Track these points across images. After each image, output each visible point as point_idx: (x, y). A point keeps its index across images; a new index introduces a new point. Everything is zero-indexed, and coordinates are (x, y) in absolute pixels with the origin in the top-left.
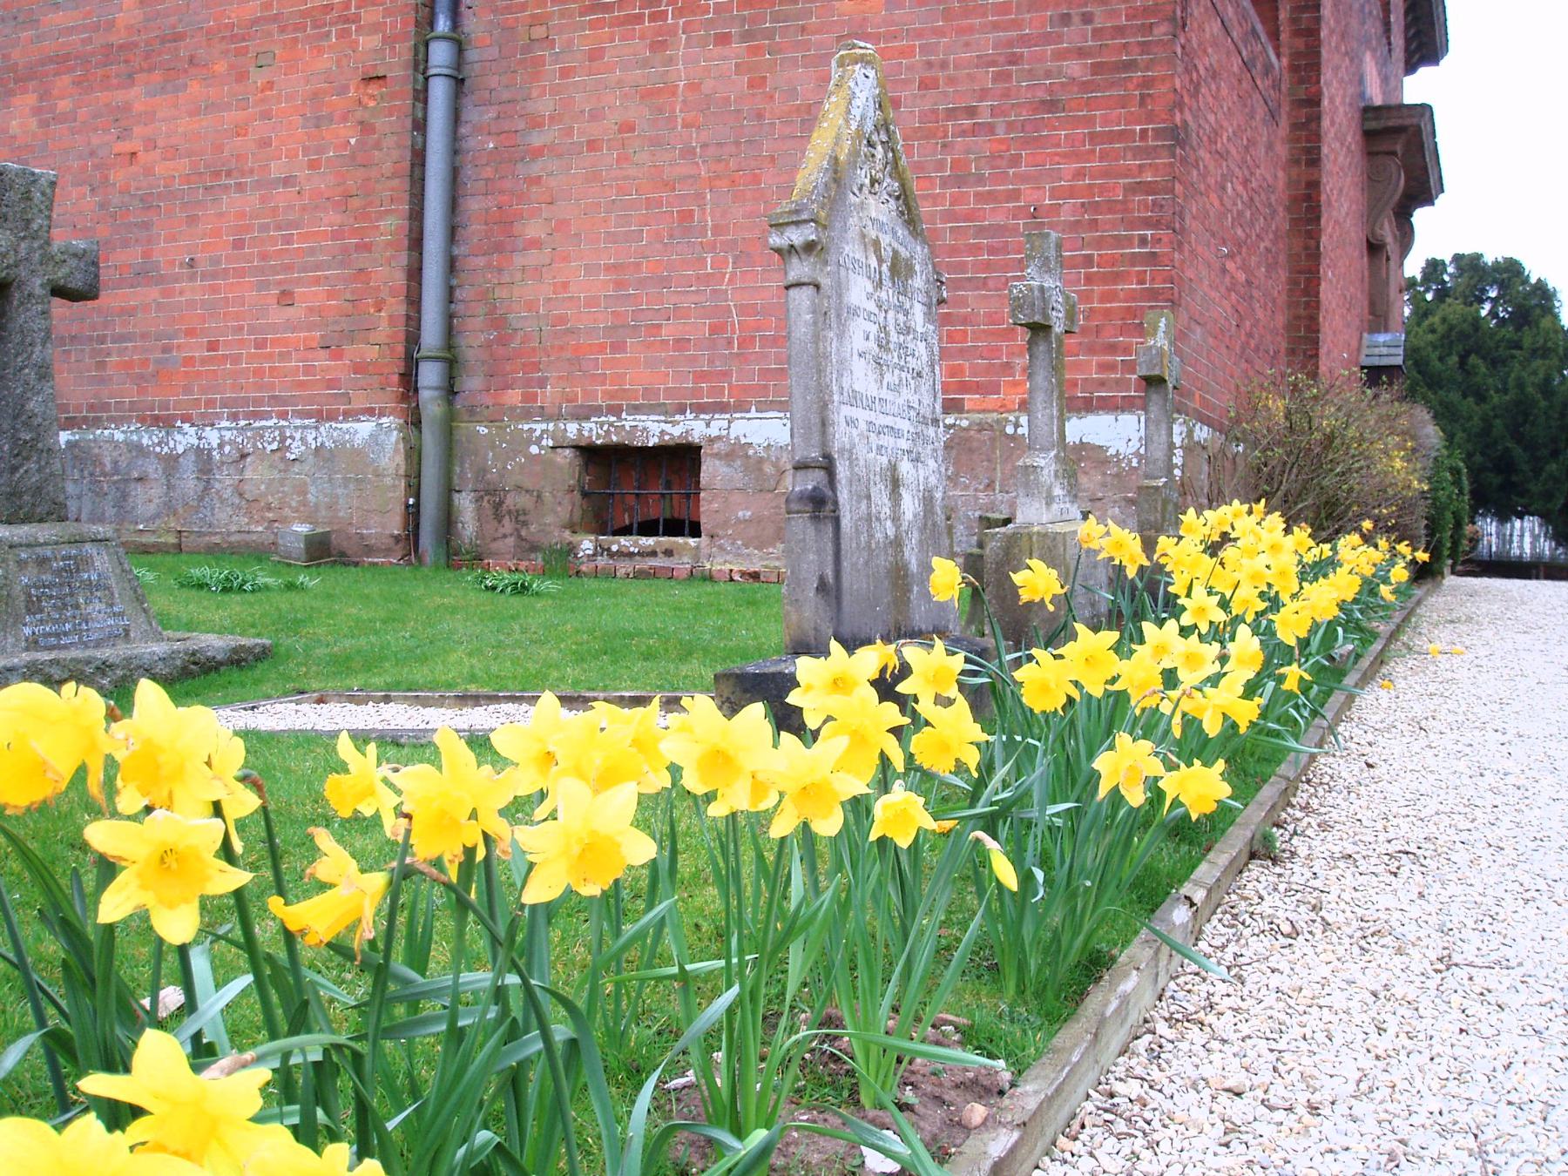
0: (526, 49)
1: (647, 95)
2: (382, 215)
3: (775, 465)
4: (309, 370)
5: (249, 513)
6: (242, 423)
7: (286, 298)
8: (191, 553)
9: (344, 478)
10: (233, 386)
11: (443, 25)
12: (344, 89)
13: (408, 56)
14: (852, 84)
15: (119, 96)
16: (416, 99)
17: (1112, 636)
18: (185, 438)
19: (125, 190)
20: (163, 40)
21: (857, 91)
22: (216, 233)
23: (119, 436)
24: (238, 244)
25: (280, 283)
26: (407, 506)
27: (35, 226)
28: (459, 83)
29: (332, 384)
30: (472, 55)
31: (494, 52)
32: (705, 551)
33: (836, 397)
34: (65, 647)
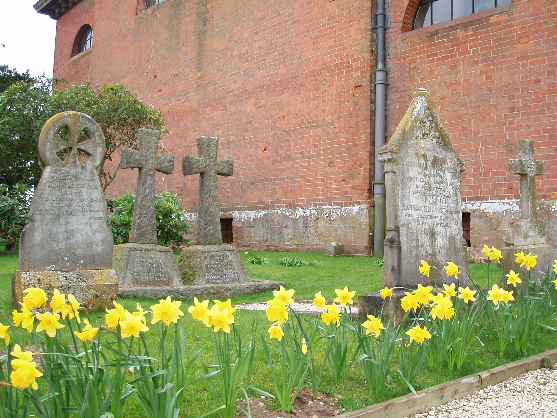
0: (409, 72)
1: (450, 85)
2: (361, 134)
3: (497, 220)
4: (338, 189)
5: (319, 238)
6: (318, 207)
7: (331, 164)
8: (301, 252)
9: (349, 226)
10: (315, 195)
11: (380, 66)
12: (349, 91)
13: (369, 78)
14: (415, 103)
15: (279, 98)
16: (371, 93)
17: (430, 288)
18: (300, 213)
19: (281, 130)
20: (292, 78)
21: (417, 105)
22: (309, 142)
23: (279, 212)
24: (316, 146)
25: (329, 159)
26: (370, 236)
27: (212, 155)
28: (386, 86)
29: (346, 193)
30: (391, 75)
31: (398, 74)
32: (472, 252)
33: (400, 208)
34: (218, 283)
